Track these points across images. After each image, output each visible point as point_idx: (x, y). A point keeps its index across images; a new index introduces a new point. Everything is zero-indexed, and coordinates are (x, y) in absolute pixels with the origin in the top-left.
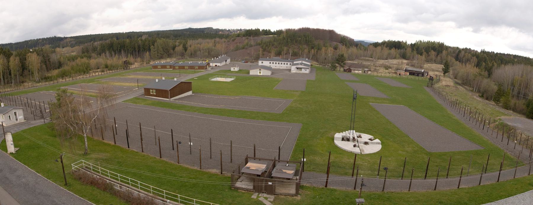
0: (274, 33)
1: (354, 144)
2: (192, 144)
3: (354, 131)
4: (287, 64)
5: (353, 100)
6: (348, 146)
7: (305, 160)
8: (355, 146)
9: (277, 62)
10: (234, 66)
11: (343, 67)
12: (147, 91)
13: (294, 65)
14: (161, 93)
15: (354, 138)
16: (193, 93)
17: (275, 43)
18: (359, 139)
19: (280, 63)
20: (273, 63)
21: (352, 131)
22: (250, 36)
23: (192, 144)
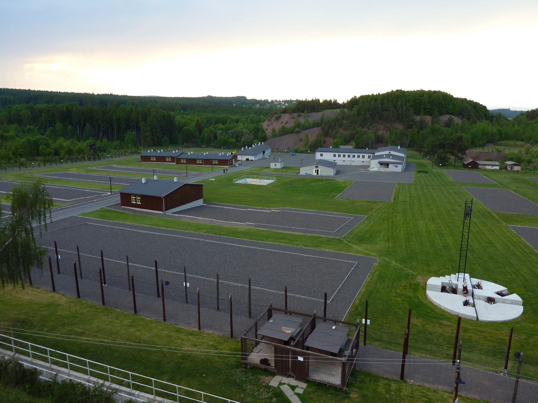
0: (344, 106)
1: (464, 299)
2: (188, 285)
3: (467, 276)
4: (363, 157)
5: (465, 218)
6: (452, 304)
7: (369, 322)
8: (466, 303)
9: (347, 155)
10: (275, 161)
11: (461, 159)
12: (126, 199)
13: (375, 157)
14: (151, 202)
15: (465, 288)
16: (204, 202)
17: (344, 122)
18: (477, 291)
19: (352, 155)
20: (339, 156)
21: (461, 275)
22: (303, 112)
23: (188, 285)
